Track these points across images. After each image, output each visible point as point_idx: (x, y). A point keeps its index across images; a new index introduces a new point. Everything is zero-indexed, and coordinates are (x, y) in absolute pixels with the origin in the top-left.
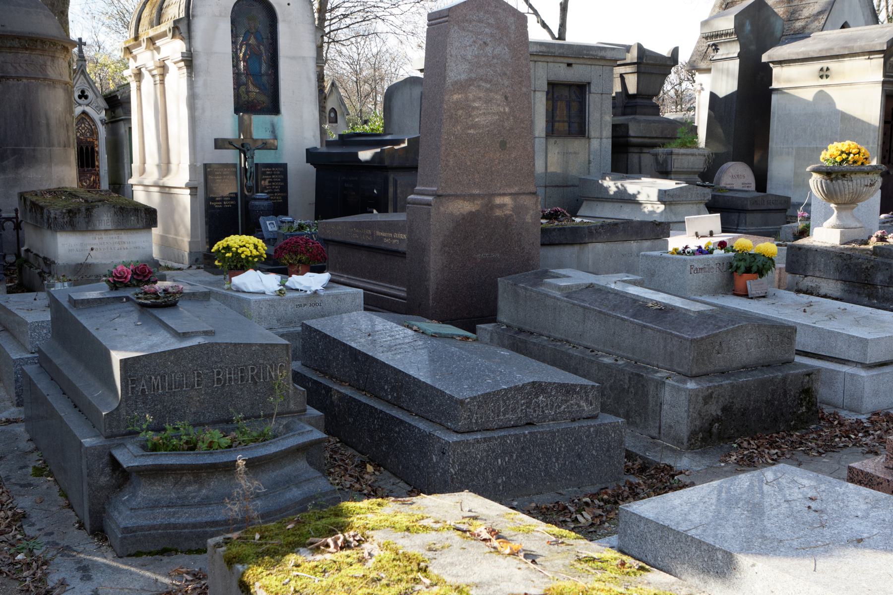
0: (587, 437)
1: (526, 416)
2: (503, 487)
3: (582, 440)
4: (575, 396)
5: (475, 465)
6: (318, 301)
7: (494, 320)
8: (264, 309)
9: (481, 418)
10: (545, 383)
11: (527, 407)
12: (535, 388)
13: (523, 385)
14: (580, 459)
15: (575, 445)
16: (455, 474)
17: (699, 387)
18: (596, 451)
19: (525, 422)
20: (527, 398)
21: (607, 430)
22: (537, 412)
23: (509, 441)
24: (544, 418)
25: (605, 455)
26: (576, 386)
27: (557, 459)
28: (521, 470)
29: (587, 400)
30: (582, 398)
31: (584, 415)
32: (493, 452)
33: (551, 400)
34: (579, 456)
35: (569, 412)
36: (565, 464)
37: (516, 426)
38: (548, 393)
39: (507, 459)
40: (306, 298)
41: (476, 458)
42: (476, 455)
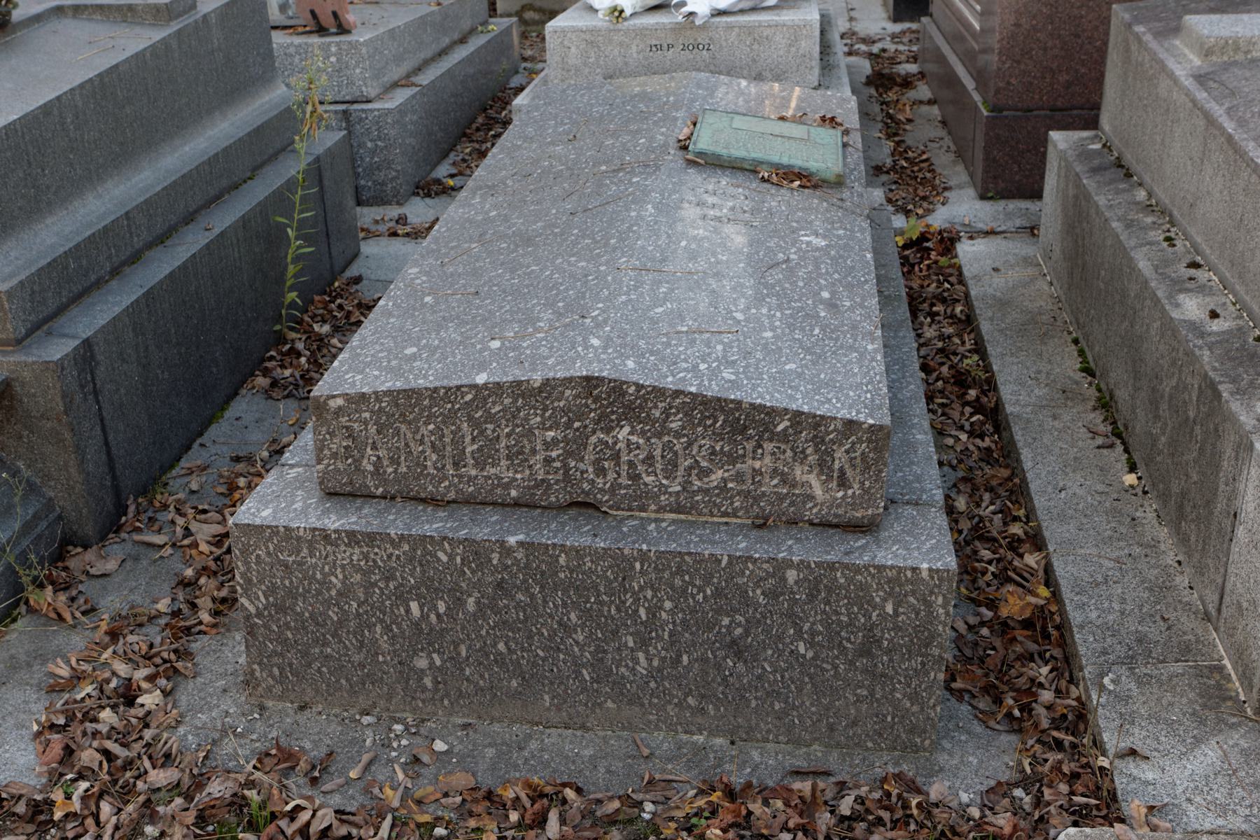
0: (772, 595)
1: (567, 477)
2: (436, 682)
3: (747, 602)
4: (768, 446)
5: (328, 603)
6: (702, 38)
7: (1092, 123)
8: (573, 50)
9: (395, 461)
10: (639, 387)
11: (568, 454)
12: (597, 399)
13: (546, 382)
14: (739, 655)
15: (719, 611)
16: (259, 614)
17: (230, 784)
18: (811, 644)
19: (564, 498)
20: (568, 425)
21: (863, 587)
22: (611, 476)
23: (444, 558)
24: (640, 499)
25: (852, 663)
26: (772, 412)
27: (643, 643)
28: (501, 646)
29: (823, 466)
30: (800, 456)
31: (811, 512)
32: (387, 579)
33: (668, 447)
34: (736, 648)
35: (746, 494)
36: (678, 660)
37: (532, 506)
38: (649, 419)
39: (442, 607)
40: (673, 30)
41: (325, 584)
42: (325, 575)
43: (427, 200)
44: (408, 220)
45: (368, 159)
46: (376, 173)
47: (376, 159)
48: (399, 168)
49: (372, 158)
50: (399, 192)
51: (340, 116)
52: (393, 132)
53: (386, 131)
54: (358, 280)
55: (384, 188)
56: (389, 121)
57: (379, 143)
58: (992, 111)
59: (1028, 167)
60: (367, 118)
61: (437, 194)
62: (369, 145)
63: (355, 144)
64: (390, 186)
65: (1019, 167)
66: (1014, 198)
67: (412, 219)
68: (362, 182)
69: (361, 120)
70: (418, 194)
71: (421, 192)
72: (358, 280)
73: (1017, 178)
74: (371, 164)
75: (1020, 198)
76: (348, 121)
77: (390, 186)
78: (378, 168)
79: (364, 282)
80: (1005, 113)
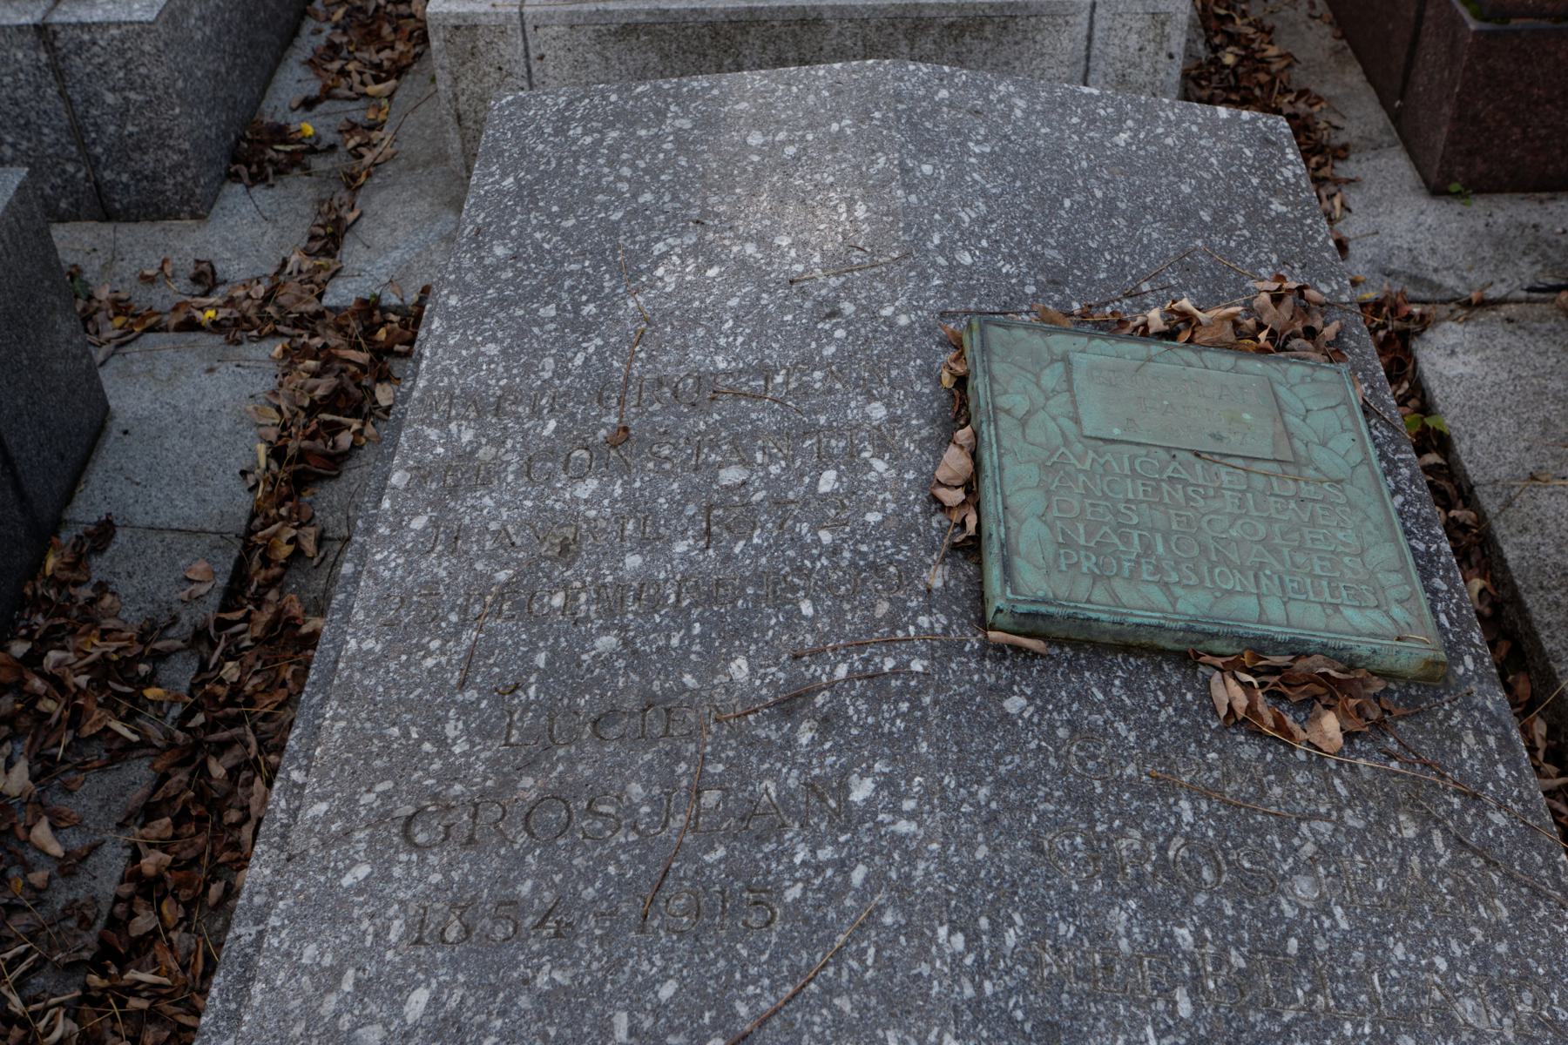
43: (259, 192)
44: (219, 276)
45: (112, 129)
46: (136, 156)
47: (130, 128)
48: (187, 146)
49: (122, 126)
50: (193, 194)
51: (29, 38)
52: (160, 73)
53: (143, 70)
54: (104, 532)
55: (159, 186)
56: (147, 48)
57: (132, 95)
58: (1486, 20)
59: (1543, 132)
60: (94, 43)
61: (279, 172)
62: (110, 98)
63: (77, 97)
64: (170, 181)
65: (1524, 131)
66: (1500, 190)
67: (234, 269)
68: (108, 175)
69: (81, 45)
70: (235, 177)
71: (243, 171)
72: (104, 532)
73: (1515, 153)
74: (121, 138)
75: (1514, 190)
76: (51, 48)
77: (170, 181)
78: (138, 147)
79: (121, 537)
80: (1515, 23)
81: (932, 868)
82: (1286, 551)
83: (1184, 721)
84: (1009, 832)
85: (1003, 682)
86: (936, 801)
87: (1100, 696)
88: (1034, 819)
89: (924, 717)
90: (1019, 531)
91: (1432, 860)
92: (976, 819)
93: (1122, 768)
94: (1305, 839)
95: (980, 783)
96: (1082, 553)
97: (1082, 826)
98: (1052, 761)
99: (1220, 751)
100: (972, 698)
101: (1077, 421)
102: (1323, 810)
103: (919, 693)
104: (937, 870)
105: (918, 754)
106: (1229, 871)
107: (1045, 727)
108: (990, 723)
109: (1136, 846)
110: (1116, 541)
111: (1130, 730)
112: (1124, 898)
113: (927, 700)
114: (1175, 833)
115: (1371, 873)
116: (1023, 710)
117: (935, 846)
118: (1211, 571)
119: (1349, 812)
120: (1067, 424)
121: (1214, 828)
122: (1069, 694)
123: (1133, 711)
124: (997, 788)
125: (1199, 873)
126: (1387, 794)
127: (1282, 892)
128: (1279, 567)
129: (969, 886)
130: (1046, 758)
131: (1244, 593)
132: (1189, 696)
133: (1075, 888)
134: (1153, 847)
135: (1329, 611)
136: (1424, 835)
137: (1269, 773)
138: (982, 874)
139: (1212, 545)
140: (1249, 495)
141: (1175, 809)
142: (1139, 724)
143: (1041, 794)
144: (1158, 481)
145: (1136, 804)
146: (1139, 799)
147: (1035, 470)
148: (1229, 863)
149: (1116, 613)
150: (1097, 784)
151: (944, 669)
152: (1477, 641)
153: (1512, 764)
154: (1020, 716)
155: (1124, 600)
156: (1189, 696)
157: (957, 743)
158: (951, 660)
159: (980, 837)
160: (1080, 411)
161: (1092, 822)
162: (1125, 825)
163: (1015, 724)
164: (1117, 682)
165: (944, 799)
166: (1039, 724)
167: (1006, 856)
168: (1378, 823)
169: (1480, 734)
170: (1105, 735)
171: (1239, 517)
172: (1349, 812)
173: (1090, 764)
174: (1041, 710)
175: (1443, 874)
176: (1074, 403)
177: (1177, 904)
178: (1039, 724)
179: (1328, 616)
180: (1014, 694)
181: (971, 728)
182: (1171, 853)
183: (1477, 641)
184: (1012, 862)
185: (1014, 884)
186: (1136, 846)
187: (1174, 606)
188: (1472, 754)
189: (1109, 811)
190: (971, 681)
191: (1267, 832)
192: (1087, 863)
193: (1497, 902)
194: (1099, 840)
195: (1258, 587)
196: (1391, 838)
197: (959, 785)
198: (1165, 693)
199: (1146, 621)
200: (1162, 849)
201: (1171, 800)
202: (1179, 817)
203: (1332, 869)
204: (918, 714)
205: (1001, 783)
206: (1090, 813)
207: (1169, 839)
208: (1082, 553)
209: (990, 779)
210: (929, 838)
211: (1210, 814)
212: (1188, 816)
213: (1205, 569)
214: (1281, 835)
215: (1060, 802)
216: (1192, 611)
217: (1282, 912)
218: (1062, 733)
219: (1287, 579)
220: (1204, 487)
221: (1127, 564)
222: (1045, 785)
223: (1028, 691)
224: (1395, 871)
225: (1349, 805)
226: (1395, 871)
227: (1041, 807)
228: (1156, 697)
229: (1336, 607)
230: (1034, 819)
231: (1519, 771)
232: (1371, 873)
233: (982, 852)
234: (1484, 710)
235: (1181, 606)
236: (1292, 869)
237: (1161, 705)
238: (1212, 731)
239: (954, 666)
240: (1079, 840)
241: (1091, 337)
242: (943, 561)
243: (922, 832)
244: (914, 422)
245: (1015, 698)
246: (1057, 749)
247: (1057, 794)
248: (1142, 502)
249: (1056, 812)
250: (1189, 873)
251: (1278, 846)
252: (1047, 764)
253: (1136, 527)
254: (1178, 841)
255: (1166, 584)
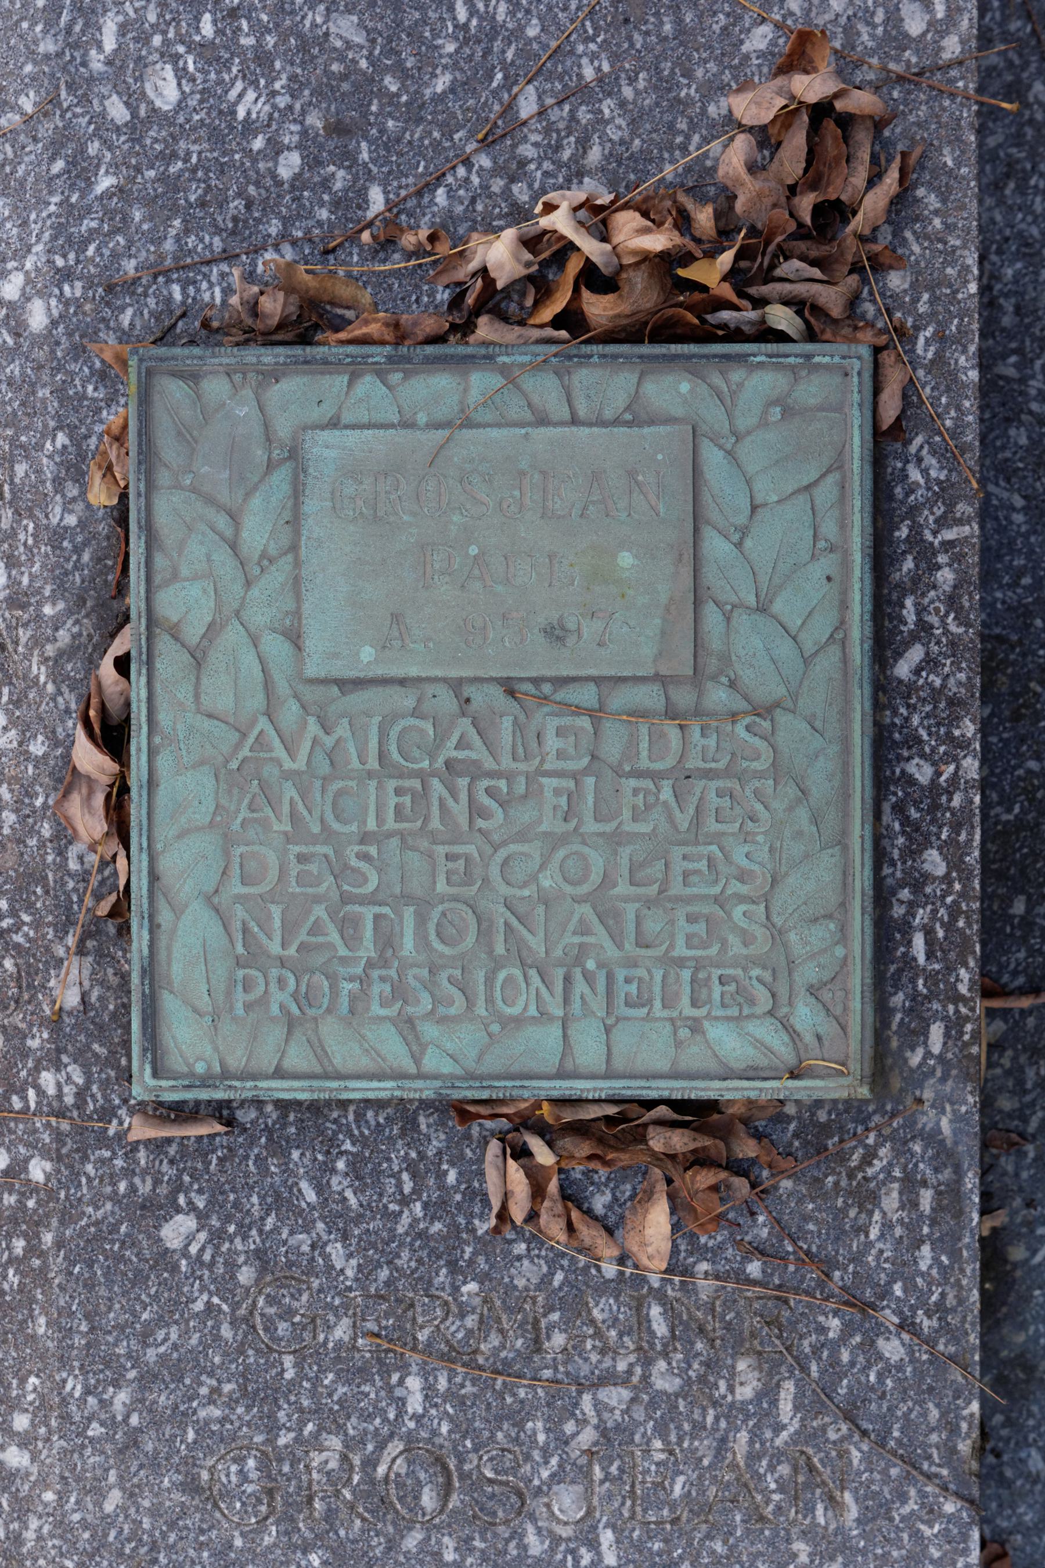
81: (46, 1529)
82: (630, 911)
83: (437, 1227)
84: (154, 1464)
85: (163, 1190)
86: (54, 1423)
87: (311, 1196)
88: (191, 1435)
89: (44, 1269)
90: (174, 931)
91: (768, 1434)
92: (109, 1448)
93: (329, 1328)
94: (582, 1422)
95: (116, 1384)
96: (274, 973)
97: (259, 1439)
98: (226, 1332)
99: (482, 1279)
100: (114, 1228)
101: (295, 638)
102: (622, 1366)
103: (39, 1223)
104: (52, 1536)
105: (34, 1337)
106: (462, 1490)
107: (220, 1270)
108: (138, 1272)
109: (333, 1465)
110: (335, 937)
111: (350, 1256)
112: (305, 1552)
113: (48, 1238)
114: (392, 1435)
115: (670, 1469)
116: (190, 1239)
117: (49, 1496)
118: (490, 981)
119: (662, 1365)
120: (276, 647)
121: (451, 1419)
122: (262, 1198)
123: (359, 1219)
124: (143, 1388)
125: (417, 1498)
126: (728, 1326)
127: (533, 1517)
128: (611, 951)
129: (91, 1557)
130: (217, 1327)
131: (544, 1017)
132: (452, 1177)
133: (238, 1542)
134: (357, 1460)
135: (684, 1033)
136: (769, 1393)
137: (551, 1309)
138: (113, 1534)
139: (500, 915)
140: (590, 781)
141: (399, 1392)
142: (367, 1242)
143: (204, 1391)
144: (423, 776)
145: (342, 1390)
146: (348, 1382)
147: (209, 782)
148: (463, 1476)
149: (321, 1090)
150: (288, 1361)
151: (75, 1174)
152: (963, 989)
153: (946, 1243)
154: (185, 1253)
155: (337, 1061)
156: (452, 1177)
157: (87, 1316)
158: (85, 1158)
159: (112, 1477)
160: (307, 607)
161: (273, 1429)
162: (320, 1429)
163: (175, 1268)
164: (341, 1165)
165: (65, 1418)
166: (213, 1263)
167: (146, 1503)
168: (702, 1379)
169: (911, 1184)
170: (311, 1270)
171: (563, 840)
172: (662, 1365)
173: (283, 1328)
174: (217, 1237)
175: (777, 1457)
176: (296, 583)
177: (378, 1552)
178: (213, 1263)
179: (678, 1044)
180: (178, 1210)
181: (110, 1283)
182: (381, 1470)
183: (963, 989)
184: (154, 1512)
185: (154, 1547)
186: (333, 1465)
187: (417, 1061)
188: (887, 1226)
189: (301, 1410)
190: (114, 1197)
191: (530, 1417)
192: (259, 1501)
193: (848, 1497)
194: (280, 1460)
195: (566, 1001)
196: (715, 1404)
197: (88, 1391)
198: (414, 1176)
199: (371, 1095)
200: (370, 1463)
201: (395, 1378)
202: (401, 1403)
203: (614, 1469)
204: (36, 1263)
205: (148, 1379)
206: (272, 1416)
207: (381, 1446)
208: (274, 973)
209: (132, 1374)
210: (43, 1483)
211: (450, 1395)
212: (415, 1404)
213: (480, 976)
214: (549, 1419)
215: (231, 1403)
216: (447, 1067)
217: (525, 1548)
218: (246, 1275)
219: (620, 974)
220: (510, 777)
221: (347, 986)
222: (211, 1374)
223: (201, 1203)
224: (706, 1462)
225: (665, 1355)
226: (706, 1462)
227: (202, 1414)
228: (399, 1185)
229: (696, 1027)
230: (191, 1435)
231: (955, 1255)
232: (670, 1469)
233: (113, 1500)
234: (932, 1137)
235: (431, 1062)
236: (553, 1476)
237: (405, 1201)
238: (478, 1239)
239: (89, 1168)
240: (251, 1463)
241: (355, 371)
242: (81, 951)
243: (35, 1470)
244: (48, 610)
245: (180, 1218)
246: (235, 1306)
247: (227, 1388)
248: (390, 835)
249: (223, 1421)
250: (400, 1499)
251: (541, 1438)
252: (217, 1338)
253: (371, 900)
254: (395, 1447)
255: (410, 1021)
